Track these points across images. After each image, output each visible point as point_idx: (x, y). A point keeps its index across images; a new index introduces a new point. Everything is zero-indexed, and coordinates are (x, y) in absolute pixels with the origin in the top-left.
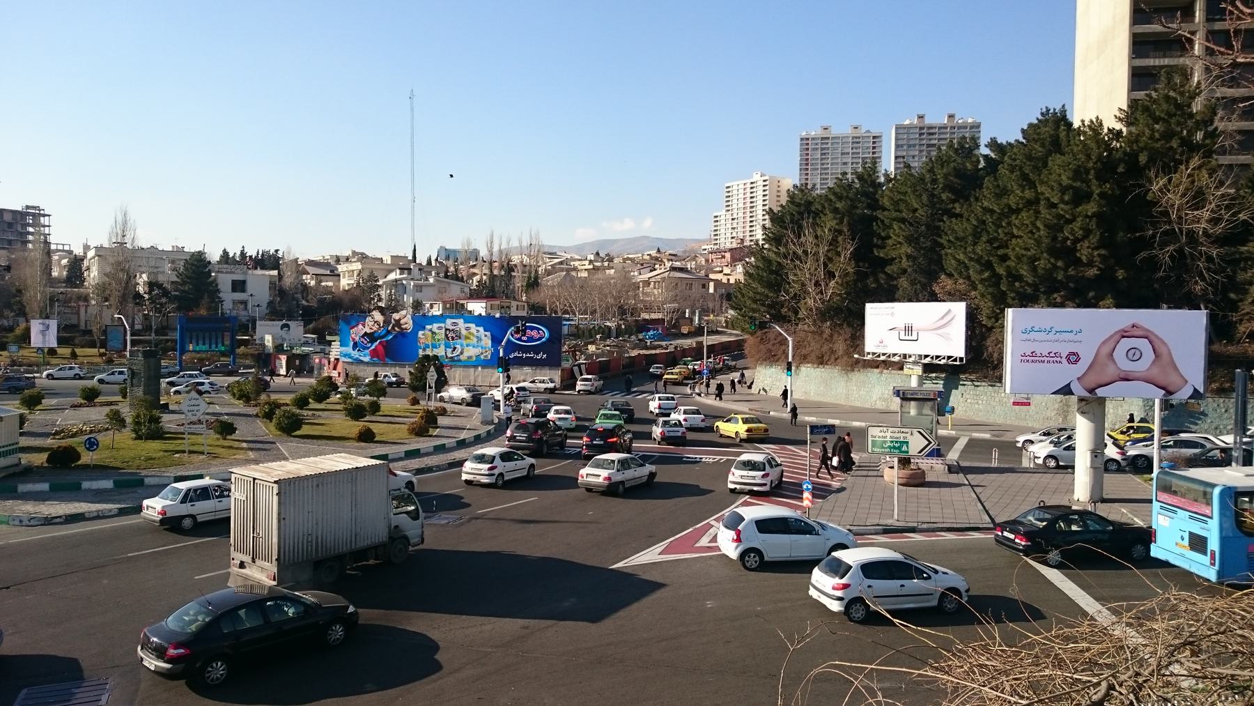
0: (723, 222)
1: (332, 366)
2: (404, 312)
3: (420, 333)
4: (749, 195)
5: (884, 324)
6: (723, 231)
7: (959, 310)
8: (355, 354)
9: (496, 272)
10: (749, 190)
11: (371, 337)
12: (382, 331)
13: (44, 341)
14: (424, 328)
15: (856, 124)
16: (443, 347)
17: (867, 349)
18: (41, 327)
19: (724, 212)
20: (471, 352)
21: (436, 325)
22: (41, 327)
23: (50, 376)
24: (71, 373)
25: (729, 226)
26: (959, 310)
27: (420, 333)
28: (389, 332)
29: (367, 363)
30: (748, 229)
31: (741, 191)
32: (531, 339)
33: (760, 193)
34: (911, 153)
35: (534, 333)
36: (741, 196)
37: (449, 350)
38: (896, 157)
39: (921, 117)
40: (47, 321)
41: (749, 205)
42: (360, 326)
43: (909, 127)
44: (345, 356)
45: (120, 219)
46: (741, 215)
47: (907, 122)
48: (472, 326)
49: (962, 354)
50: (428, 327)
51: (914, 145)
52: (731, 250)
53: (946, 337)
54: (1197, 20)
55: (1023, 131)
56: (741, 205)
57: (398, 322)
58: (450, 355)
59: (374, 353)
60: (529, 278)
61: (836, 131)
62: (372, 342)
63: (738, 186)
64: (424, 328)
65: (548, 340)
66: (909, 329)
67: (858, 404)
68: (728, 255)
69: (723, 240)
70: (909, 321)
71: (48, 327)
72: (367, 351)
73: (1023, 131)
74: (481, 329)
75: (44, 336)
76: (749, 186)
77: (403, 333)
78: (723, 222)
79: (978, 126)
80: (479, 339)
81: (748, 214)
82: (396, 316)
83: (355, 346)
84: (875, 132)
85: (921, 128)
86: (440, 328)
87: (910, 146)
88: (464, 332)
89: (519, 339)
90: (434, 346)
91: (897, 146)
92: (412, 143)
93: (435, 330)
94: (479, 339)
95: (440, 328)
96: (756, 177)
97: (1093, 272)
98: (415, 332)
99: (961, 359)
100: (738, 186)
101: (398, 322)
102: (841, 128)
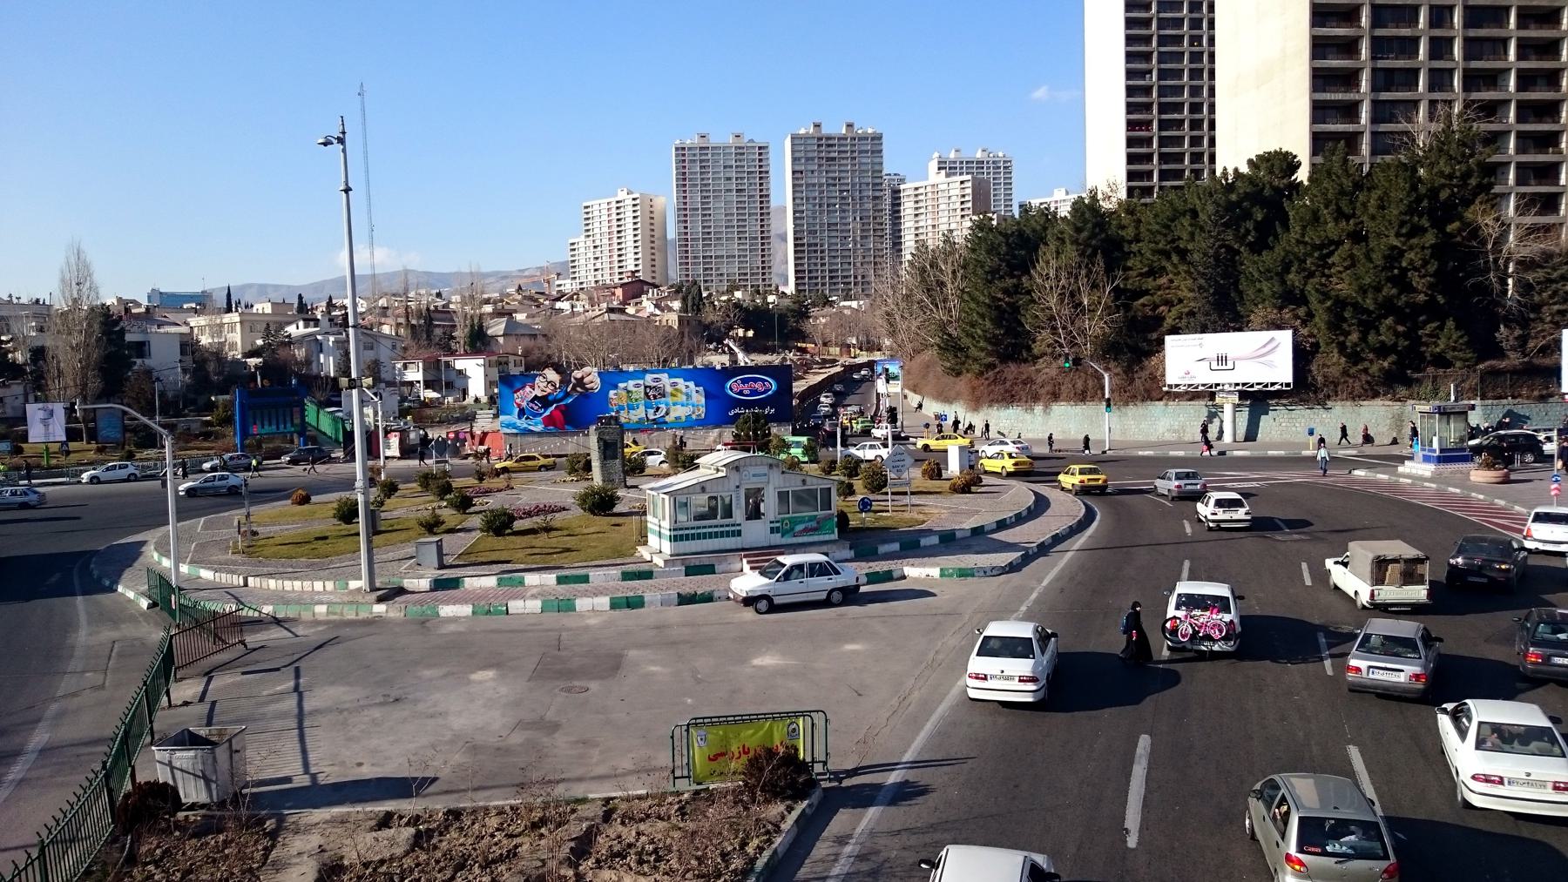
0: (582, 250)
1: (477, 440)
2: (587, 369)
3: (612, 393)
4: (614, 217)
5: (1186, 357)
6: (582, 262)
7: (1285, 338)
8: (522, 423)
9: (414, 322)
10: (614, 211)
11: (544, 401)
12: (559, 394)
13: (47, 434)
14: (616, 387)
15: (738, 132)
16: (642, 408)
17: (1169, 382)
18: (41, 414)
19: (583, 238)
20: (679, 412)
21: (631, 383)
22: (41, 414)
23: (94, 480)
24: (123, 473)
25: (590, 255)
26: (1285, 338)
27: (612, 393)
28: (567, 395)
29: (539, 434)
30: (616, 258)
31: (605, 212)
32: (754, 392)
33: (630, 214)
34: (810, 168)
35: (758, 386)
36: (605, 218)
37: (651, 411)
38: (794, 172)
39: (817, 126)
40: (50, 406)
41: (615, 229)
42: (528, 389)
43: (806, 137)
44: (508, 426)
45: (73, 260)
46: (605, 241)
47: (802, 131)
48: (680, 381)
49: (1290, 380)
50: (622, 385)
51: (813, 159)
52: (622, 285)
53: (1270, 365)
54: (1363, 57)
55: (1250, 162)
56: (605, 229)
57: (580, 382)
58: (651, 417)
59: (548, 421)
60: (472, 326)
61: (715, 140)
62: (546, 407)
63: (599, 206)
64: (616, 387)
65: (775, 393)
66: (1222, 359)
67: (1140, 438)
68: (619, 292)
69: (583, 273)
70: (1222, 352)
71: (51, 413)
72: (539, 419)
73: (1250, 162)
74: (691, 384)
75: (46, 426)
76: (614, 205)
77: (587, 394)
78: (582, 250)
79: (880, 138)
80: (688, 396)
81: (615, 241)
82: (578, 374)
83: (522, 412)
84: (760, 141)
85: (820, 139)
86: (637, 386)
87: (808, 159)
88: (669, 389)
89: (741, 393)
90: (631, 408)
91: (794, 160)
92: (366, 153)
93: (631, 388)
94: (688, 396)
95: (637, 386)
96: (622, 195)
97: (1422, 297)
98: (604, 392)
99: (1288, 385)
100: (599, 206)
101: (580, 382)
102: (721, 136)
